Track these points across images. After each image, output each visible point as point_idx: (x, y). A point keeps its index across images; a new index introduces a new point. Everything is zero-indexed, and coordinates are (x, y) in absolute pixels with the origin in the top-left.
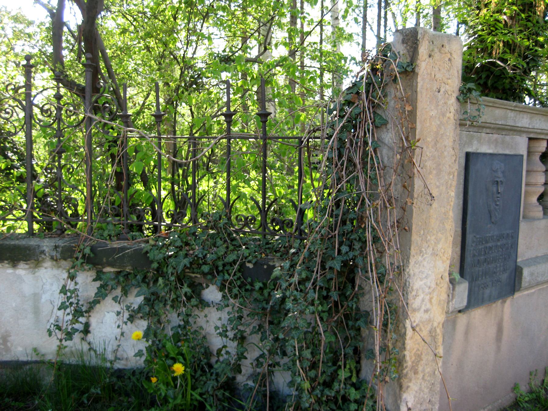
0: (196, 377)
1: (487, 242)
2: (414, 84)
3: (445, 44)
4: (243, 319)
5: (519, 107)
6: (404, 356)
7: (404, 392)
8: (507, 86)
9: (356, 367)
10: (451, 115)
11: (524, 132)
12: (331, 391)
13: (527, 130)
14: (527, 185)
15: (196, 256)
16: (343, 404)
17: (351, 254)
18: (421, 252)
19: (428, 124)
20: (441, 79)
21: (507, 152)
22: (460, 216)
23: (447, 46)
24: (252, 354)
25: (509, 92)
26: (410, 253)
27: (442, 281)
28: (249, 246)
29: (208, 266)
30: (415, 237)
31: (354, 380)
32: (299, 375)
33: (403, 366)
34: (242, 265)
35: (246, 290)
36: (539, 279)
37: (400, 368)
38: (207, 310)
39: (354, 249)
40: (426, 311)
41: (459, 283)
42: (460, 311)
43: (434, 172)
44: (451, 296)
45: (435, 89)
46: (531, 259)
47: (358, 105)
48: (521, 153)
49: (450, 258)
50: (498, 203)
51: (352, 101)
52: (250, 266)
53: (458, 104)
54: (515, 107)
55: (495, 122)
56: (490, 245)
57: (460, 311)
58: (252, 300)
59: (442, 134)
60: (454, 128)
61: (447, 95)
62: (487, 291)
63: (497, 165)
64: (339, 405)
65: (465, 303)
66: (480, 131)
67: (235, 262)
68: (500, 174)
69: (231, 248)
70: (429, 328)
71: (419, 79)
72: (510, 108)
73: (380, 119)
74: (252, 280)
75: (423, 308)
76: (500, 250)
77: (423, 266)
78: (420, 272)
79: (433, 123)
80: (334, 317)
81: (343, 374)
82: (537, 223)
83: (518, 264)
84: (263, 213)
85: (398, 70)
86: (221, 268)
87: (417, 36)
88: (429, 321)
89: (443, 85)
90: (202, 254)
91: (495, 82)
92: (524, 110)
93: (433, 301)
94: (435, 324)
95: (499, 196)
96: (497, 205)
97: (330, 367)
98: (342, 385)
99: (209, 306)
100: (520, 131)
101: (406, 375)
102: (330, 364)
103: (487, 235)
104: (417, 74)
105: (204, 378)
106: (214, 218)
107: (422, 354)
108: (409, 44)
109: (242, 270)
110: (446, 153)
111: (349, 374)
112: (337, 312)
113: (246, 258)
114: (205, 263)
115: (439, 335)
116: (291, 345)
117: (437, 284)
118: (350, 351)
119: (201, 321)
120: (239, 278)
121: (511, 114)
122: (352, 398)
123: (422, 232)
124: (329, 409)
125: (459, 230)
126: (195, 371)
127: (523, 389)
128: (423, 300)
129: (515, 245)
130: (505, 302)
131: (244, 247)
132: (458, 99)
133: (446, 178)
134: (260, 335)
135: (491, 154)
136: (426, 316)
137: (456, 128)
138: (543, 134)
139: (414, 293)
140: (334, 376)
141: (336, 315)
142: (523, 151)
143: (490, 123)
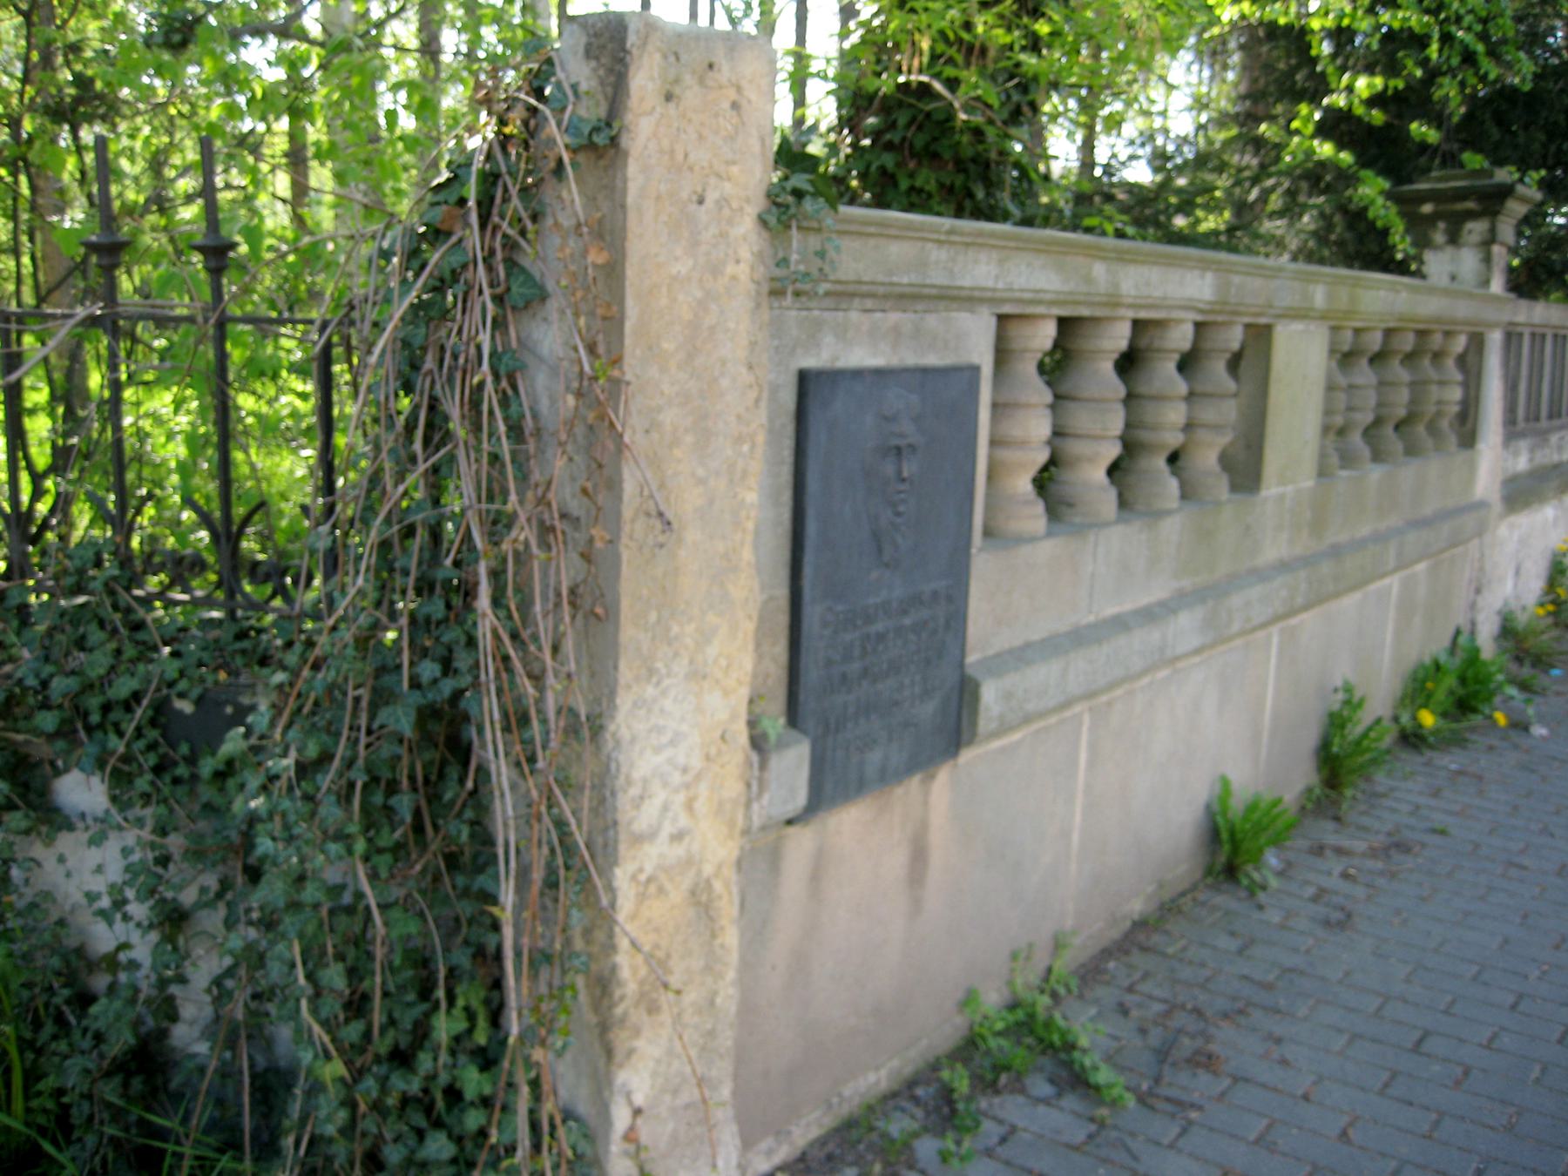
0: (39, 1044)
1: (869, 619)
2: (619, 183)
3: (720, 58)
4: (171, 866)
5: (962, 234)
6: (614, 969)
7: (621, 1066)
8: (968, 152)
9: (487, 1002)
10: (743, 271)
11: (982, 301)
12: (410, 1077)
13: (989, 294)
14: (994, 443)
15: (20, 681)
16: (449, 1108)
17: (447, 686)
18: (651, 671)
19: (664, 301)
20: (705, 164)
21: (932, 360)
22: (784, 554)
23: (725, 67)
24: (205, 966)
25: (972, 167)
26: (616, 680)
27: (724, 747)
28: (182, 648)
29: (56, 712)
30: (629, 632)
31: (481, 1038)
32: (311, 1041)
33: (611, 995)
34: (161, 708)
35: (176, 781)
36: (1031, 707)
37: (605, 1002)
38: (65, 841)
39: (456, 671)
40: (678, 837)
41: (781, 745)
42: (790, 822)
43: (689, 439)
44: (756, 784)
45: (684, 195)
46: (1011, 652)
47: (460, 241)
48: (975, 360)
49: (748, 679)
50: (901, 508)
51: (444, 227)
52: (186, 707)
53: (765, 234)
54: (951, 232)
55: (887, 280)
56: (879, 627)
57: (790, 822)
58: (197, 808)
59: (712, 329)
60: (751, 305)
61: (726, 212)
62: (875, 757)
63: (896, 399)
64: (439, 1116)
65: (801, 798)
66: (844, 306)
67: (137, 696)
68: (907, 427)
69: (130, 651)
70: (687, 882)
71: (632, 168)
72: (935, 236)
73: (523, 284)
74: (192, 750)
75: (668, 829)
76: (912, 637)
77: (662, 711)
78: (650, 731)
79: (681, 297)
80: (416, 861)
81: (444, 1027)
82: (1025, 551)
83: (969, 671)
84: (223, 540)
85: (568, 140)
86: (95, 718)
87: (623, 41)
88: (689, 862)
89: (713, 181)
90: (37, 675)
91: (935, 139)
92: (980, 240)
93: (698, 805)
94: (708, 869)
95: (902, 487)
96: (898, 514)
97: (409, 1005)
98: (444, 1057)
99: (71, 827)
100: (970, 299)
101: (623, 1020)
102: (411, 997)
103: (871, 601)
104: (626, 154)
105: (63, 1046)
106: (78, 563)
107: (668, 956)
108: (603, 60)
109: (163, 720)
110: (725, 383)
111: (462, 1025)
112: (423, 846)
113: (171, 685)
114: (45, 705)
115: (720, 897)
116: (280, 958)
117: (708, 758)
118: (462, 958)
119: (51, 873)
120: (152, 747)
121: (938, 254)
122: (470, 1093)
123: (653, 616)
124: (406, 1128)
125: (782, 593)
126: (37, 1025)
127: (992, 999)
128: (666, 808)
129: (957, 620)
130: (932, 777)
131: (167, 650)
132: (763, 221)
133: (729, 452)
134: (222, 911)
135: (879, 373)
136: (679, 851)
137: (758, 306)
138: (1039, 302)
139: (634, 791)
140: (421, 1032)
141: (420, 856)
142: (982, 355)
143: (873, 283)
